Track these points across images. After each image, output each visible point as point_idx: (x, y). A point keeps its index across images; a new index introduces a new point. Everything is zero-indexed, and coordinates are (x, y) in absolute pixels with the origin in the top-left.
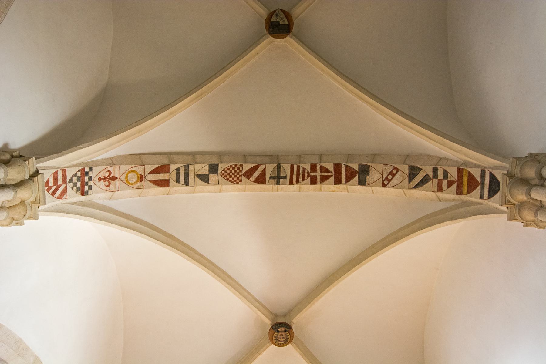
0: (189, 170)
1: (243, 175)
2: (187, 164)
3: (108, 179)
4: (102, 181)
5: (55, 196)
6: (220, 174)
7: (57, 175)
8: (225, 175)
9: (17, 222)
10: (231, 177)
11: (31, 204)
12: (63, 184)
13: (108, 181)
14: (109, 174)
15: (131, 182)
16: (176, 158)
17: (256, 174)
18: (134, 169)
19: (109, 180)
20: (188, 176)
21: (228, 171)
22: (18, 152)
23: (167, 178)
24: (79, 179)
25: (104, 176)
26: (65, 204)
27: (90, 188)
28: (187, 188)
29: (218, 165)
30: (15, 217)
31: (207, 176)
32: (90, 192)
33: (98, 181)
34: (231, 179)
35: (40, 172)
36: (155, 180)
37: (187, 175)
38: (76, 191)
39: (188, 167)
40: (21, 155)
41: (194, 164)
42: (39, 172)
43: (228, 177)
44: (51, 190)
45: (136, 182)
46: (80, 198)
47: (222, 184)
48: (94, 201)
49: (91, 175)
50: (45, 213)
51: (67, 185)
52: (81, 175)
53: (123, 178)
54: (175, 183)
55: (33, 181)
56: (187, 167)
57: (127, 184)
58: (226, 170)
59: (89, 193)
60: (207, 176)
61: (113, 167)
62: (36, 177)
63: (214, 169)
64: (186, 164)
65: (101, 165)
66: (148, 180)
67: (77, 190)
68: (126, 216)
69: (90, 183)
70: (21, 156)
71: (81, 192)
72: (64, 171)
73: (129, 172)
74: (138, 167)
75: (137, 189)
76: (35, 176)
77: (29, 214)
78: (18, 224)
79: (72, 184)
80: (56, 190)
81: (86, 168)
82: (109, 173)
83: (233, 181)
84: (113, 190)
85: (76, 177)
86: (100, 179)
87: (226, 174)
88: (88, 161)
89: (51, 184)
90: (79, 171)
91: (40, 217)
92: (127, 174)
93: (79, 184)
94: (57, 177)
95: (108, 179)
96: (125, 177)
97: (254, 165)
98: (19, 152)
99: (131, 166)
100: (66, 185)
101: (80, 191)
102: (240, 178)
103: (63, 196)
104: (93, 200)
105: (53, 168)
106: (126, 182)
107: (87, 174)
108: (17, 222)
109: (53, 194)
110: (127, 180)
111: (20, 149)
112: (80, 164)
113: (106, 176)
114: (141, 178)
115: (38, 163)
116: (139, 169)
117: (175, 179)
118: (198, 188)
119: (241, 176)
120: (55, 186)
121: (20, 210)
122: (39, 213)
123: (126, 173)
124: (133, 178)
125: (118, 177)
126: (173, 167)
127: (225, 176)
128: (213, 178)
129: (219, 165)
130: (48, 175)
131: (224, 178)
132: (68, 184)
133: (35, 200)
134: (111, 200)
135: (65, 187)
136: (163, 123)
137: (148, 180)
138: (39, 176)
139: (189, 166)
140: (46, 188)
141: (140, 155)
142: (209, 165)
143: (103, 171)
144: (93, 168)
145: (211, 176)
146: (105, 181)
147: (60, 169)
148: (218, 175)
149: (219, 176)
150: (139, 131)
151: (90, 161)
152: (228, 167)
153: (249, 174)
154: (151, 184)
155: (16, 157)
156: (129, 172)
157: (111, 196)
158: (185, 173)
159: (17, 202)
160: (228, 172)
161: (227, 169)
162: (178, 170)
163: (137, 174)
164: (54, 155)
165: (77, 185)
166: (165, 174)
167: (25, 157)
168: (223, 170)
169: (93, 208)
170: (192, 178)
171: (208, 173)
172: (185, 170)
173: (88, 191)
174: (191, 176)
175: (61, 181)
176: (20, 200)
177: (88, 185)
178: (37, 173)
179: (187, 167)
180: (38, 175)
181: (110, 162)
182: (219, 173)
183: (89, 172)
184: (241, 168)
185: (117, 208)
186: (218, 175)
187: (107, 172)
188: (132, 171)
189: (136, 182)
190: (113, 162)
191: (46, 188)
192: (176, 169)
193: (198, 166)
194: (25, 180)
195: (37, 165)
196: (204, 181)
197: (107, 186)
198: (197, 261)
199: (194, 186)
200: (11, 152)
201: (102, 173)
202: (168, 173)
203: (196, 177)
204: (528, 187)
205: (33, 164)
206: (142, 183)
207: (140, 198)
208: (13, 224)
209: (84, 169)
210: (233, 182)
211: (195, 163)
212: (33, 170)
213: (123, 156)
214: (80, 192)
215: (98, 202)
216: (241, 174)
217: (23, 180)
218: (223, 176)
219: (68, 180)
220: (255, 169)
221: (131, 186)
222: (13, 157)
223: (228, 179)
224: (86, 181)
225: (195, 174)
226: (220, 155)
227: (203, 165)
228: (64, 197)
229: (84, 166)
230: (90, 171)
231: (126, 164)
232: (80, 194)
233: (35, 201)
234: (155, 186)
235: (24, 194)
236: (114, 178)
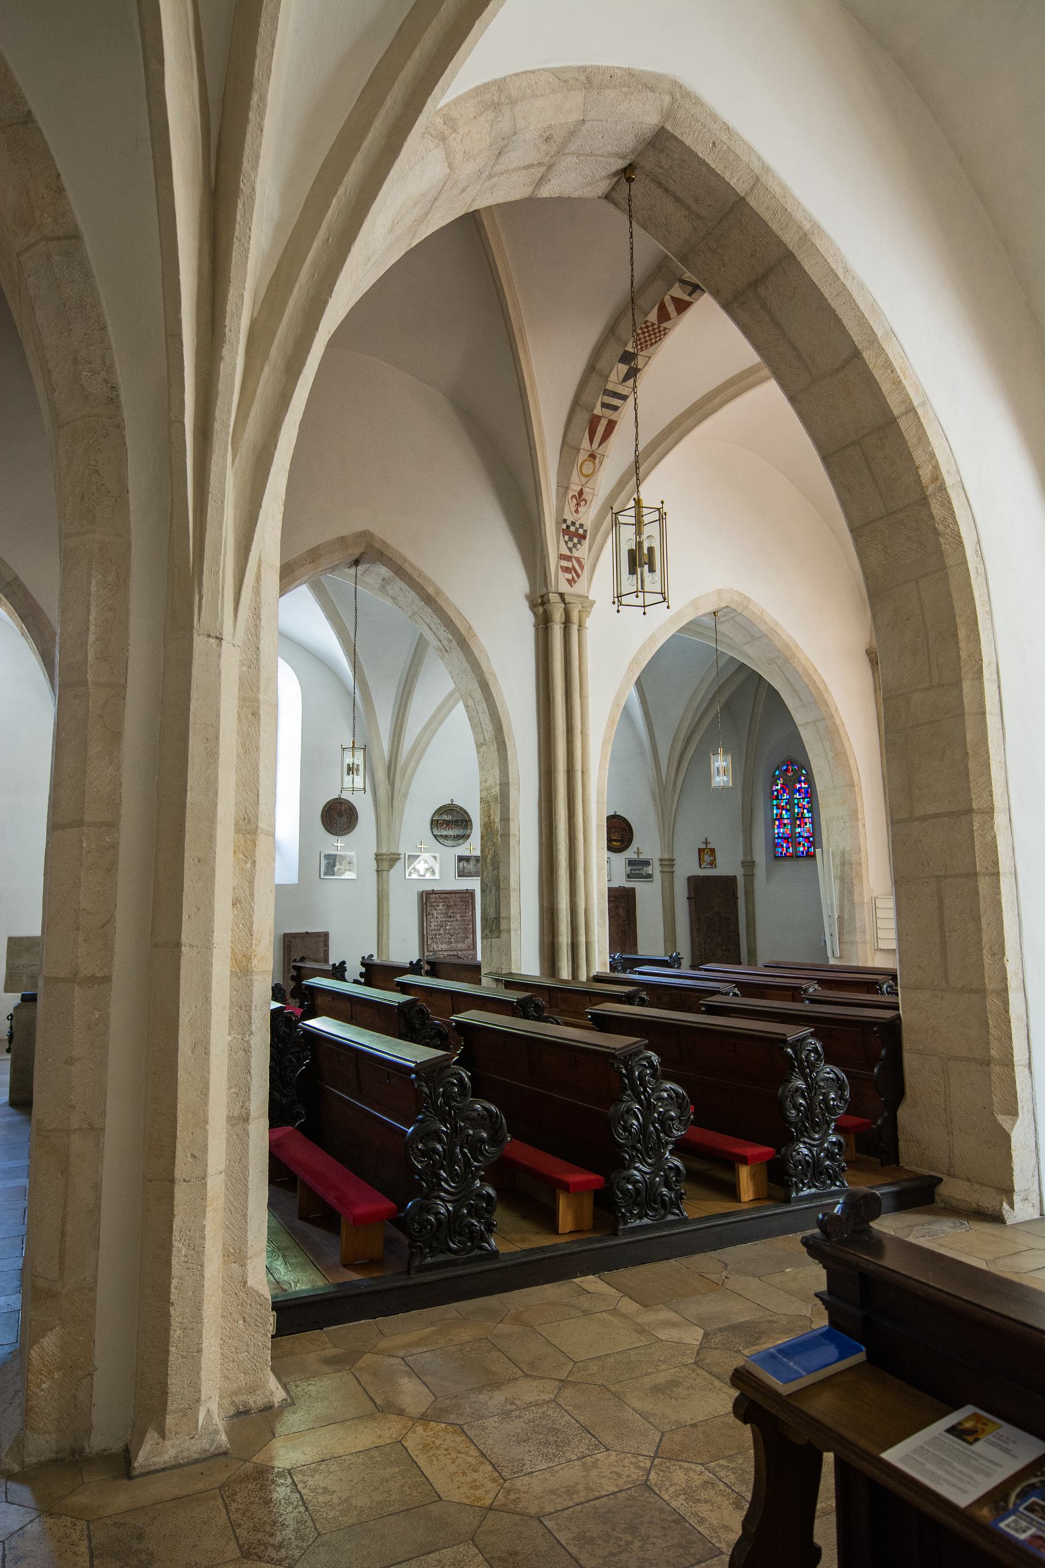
1: (659, 323)
10: (651, 340)
12: (572, 561)
16: (586, 397)
17: (671, 309)
18: (579, 464)
23: (606, 422)
24: (571, 540)
32: (585, 528)
34: (654, 341)
43: (649, 343)
45: (594, 463)
46: (586, 543)
63: (627, 358)
67: (580, 543)
80: (576, 571)
83: (658, 339)
86: (577, 511)
90: (564, 536)
92: (582, 474)
97: (656, 308)
99: (575, 467)
102: (662, 329)
105: (557, 570)
107: (568, 527)
114: (592, 457)
116: (582, 456)
117: (612, 412)
119: (659, 327)
124: (588, 468)
125: (581, 487)
126: (598, 410)
127: (646, 346)
153: (664, 316)
154: (604, 444)
162: (605, 405)
163: (586, 460)
174: (621, 390)
184: (649, 324)
188: (581, 467)
189: (594, 463)
190: (563, 487)
193: (613, 377)
197: (586, 503)
204: (223, 1438)
209: (563, 529)
210: (660, 339)
211: (606, 379)
216: (656, 326)
220: (662, 308)
223: (651, 344)
225: (620, 384)
226: (611, 332)
227: (615, 371)
234: (607, 441)
236: (581, 493)
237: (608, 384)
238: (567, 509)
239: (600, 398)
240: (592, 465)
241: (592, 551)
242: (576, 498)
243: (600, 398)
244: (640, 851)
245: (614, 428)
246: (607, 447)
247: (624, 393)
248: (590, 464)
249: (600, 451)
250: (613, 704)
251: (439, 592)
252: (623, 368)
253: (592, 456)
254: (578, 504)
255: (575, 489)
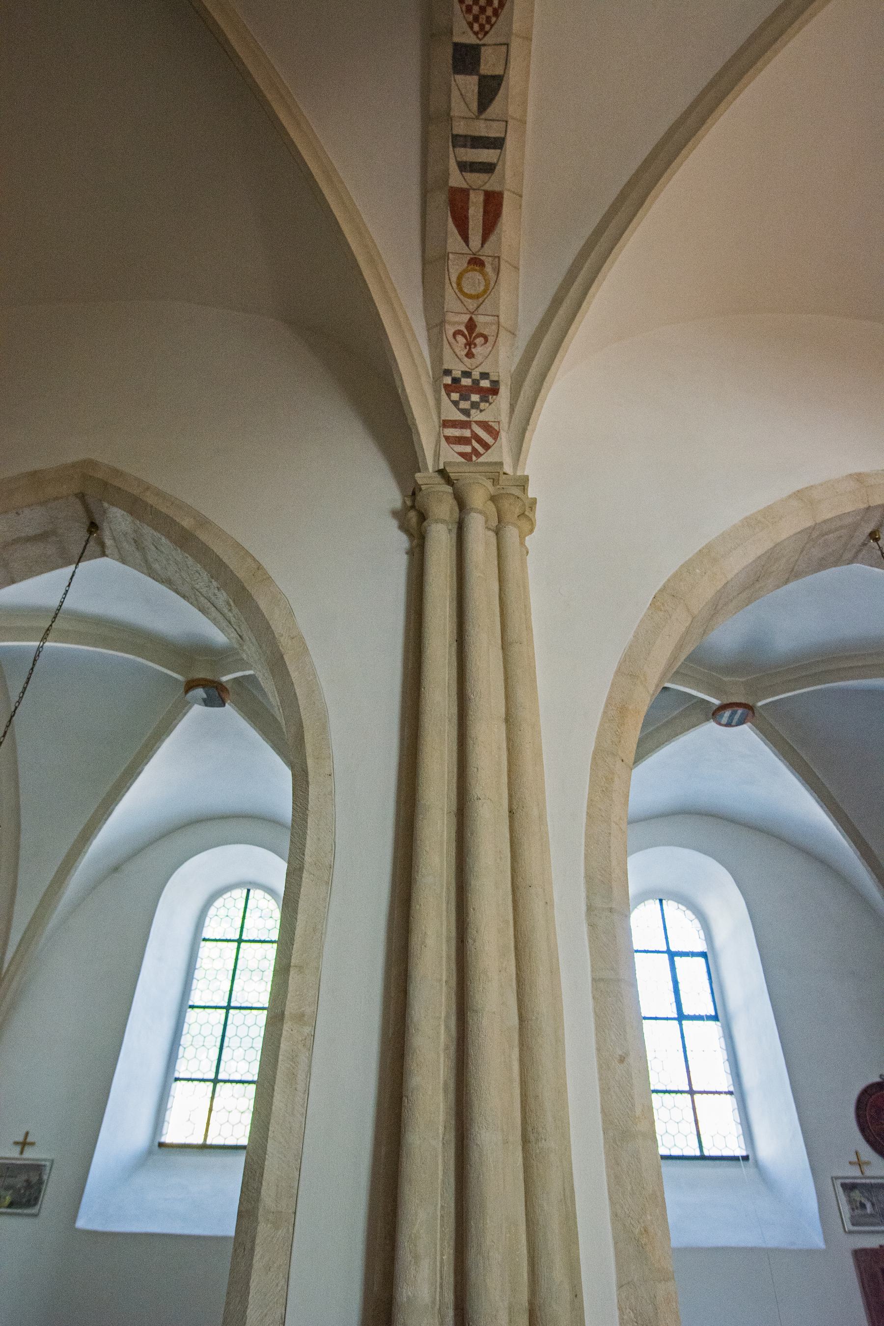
0: (466, 136)
2: (450, 140)
3: (470, 337)
4: (473, 350)
5: (491, 444)
6: (480, 40)
7: (453, 437)
8: (484, 22)
9: (527, 509)
11: (498, 486)
12: (470, 428)
13: (475, 338)
14: (460, 336)
15: (482, 288)
18: (454, 279)
19: (474, 335)
20: (481, 138)
21: (474, 11)
22: (405, 498)
23: (481, 198)
24: (465, 397)
25: (463, 346)
26: (509, 426)
27: (484, 376)
28: (509, 144)
29: (456, 46)
30: (517, 511)
31: (483, 79)
33: (473, 360)
35: (441, 467)
36: (484, 230)
37: (478, 142)
38: (488, 404)
39: (458, 138)
40: (411, 494)
41: (452, 120)
42: (442, 469)
43: (489, 11)
44: (479, 450)
47: (509, 34)
48: (513, 369)
49: (460, 373)
50: (520, 463)
51: (475, 419)
52: (457, 392)
53: (471, 304)
54: (495, 177)
55: (457, 480)
56: (460, 141)
57: (485, 296)
58: (470, 18)
59: (496, 379)
60: (483, 79)
61: (447, 326)
62: (450, 474)
64: (450, 144)
65: (442, 350)
66: (482, 246)
67: (487, 401)
68: (557, 302)
69: (476, 374)
70: (414, 494)
71: (491, 394)
72: (446, 424)
73: (461, 290)
74: (451, 270)
75: (500, 274)
76: (449, 477)
77: (516, 491)
78: (533, 508)
79: (473, 412)
80: (480, 441)
81: (444, 382)
82: (459, 334)
84: (494, 327)
85: (461, 402)
87: (483, 19)
88: (431, 376)
89: (468, 449)
90: (449, 395)
91: (526, 474)
93: (475, 398)
94: (456, 437)
95: (470, 337)
96: (470, 301)
98: (406, 496)
99: (447, 285)
100: (474, 422)
101: (488, 397)
103: (494, 429)
104: (512, 372)
105: (438, 443)
106: (481, 300)
107: (456, 380)
108: (527, 509)
109: (487, 447)
110: (477, 297)
111: (404, 496)
112: (437, 392)
113: (464, 341)
115: (427, 469)
117: (484, 177)
118: (513, 110)
120: (473, 442)
121: (506, 504)
122: (519, 473)
123: (462, 297)
124: (474, 282)
126: (456, 179)
127: (488, 19)
128: (489, 64)
129: (456, 39)
130: (450, 455)
131: (492, 26)
132: (471, 418)
133: (492, 480)
134: (517, 333)
135: (480, 426)
136: (350, 198)
137: (482, 246)
138: (448, 469)
139: (455, 132)
140: (474, 458)
141: (425, 262)
142: (454, 73)
143: (454, 347)
144: (446, 367)
145: (486, 69)
146: (475, 345)
147: (441, 431)
148: (484, 45)
149: (487, 40)
150: (372, 261)
151: (431, 373)
152: (464, 8)
154: (493, 238)
155: (414, 501)
156: (461, 290)
157: (508, 333)
158: (473, 147)
159: (491, 508)
160: (477, 13)
161: (467, 16)
162: (465, 167)
163: (465, 271)
164: (415, 439)
165: (477, 402)
166: (470, 203)
167: (414, 488)
168: (471, 28)
169: (527, 371)
170: (487, 126)
171: (476, 78)
172: (465, 146)
173: (491, 381)
174: (482, 129)
175: (464, 430)
176: (490, 503)
177: (478, 380)
178: (442, 473)
179: (460, 141)
180: (447, 472)
181: (436, 330)
182: (478, 42)
183: (453, 376)
185: (536, 323)
186: (484, 45)
187: (456, 340)
188: (459, 284)
191: (474, 458)
192: (461, 171)
193: (458, 108)
194: (454, 492)
195: (431, 470)
196: (494, 92)
197: (486, 340)
198: (703, 121)
199: (507, 122)
200: (406, 509)
201: (457, 351)
202: (468, 195)
203: (483, 116)
205: (426, 477)
206: (487, 261)
207: (521, 268)
208: (531, 516)
209: (446, 386)
211: (449, 118)
212: (438, 479)
213: (425, 302)
214: (490, 397)
215: (517, 360)
217: (453, 496)
218: (487, 27)
219: (464, 418)
221: (490, 289)
222: (413, 507)
223: (496, 13)
224: (470, 384)
225: (477, 118)
227: (455, 93)
228: (496, 428)
229: (440, 386)
230: (451, 375)
231: (443, 296)
232: (494, 397)
233: (493, 479)
234: (497, 231)
235: (478, 497)
236: (471, 325)
237: (455, 124)
238: (447, 351)
239: (452, 156)
240: (481, 278)
241: (516, 410)
242: (465, 336)
243: (452, 156)
244: (29, 1140)
245: (500, 205)
246: (499, 239)
247: (492, 135)
248: (478, 276)
249: (488, 249)
250: (619, 672)
251: (204, 522)
252: (468, 84)
253: (476, 262)
254: (470, 344)
255: (457, 320)
